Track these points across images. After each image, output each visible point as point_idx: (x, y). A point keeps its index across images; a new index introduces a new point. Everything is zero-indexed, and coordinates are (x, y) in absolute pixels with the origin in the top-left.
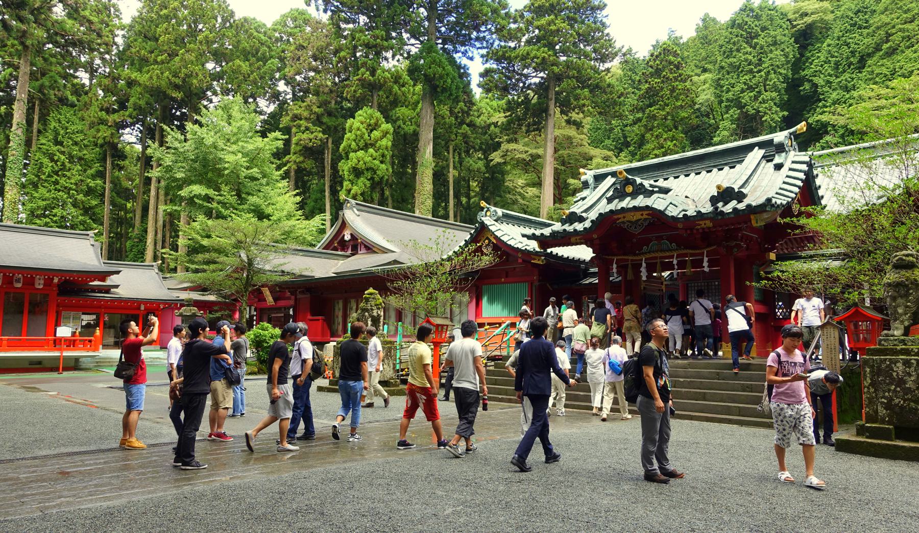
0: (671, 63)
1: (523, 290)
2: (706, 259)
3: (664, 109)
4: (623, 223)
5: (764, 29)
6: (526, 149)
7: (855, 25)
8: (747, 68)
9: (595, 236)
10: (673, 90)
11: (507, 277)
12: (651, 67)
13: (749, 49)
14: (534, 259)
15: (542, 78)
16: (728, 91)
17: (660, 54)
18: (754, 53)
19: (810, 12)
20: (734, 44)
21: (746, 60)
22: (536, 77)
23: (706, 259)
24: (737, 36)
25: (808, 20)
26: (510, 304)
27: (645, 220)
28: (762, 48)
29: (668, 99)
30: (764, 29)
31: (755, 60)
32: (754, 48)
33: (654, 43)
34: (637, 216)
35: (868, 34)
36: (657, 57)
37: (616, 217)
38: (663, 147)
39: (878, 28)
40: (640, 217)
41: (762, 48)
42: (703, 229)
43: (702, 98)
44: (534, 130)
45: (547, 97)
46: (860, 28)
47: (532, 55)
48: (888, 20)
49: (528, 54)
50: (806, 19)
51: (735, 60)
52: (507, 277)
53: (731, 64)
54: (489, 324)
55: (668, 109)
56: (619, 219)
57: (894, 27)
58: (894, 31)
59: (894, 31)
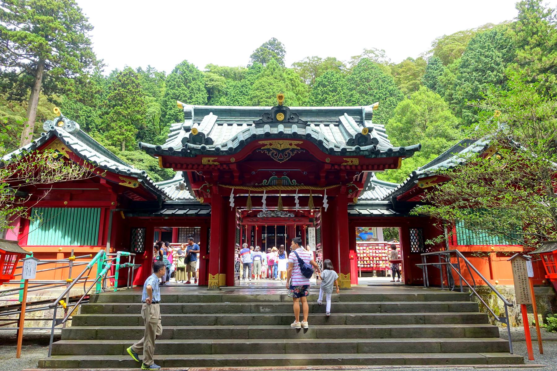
0: (133, 82)
1: (93, 216)
2: (326, 196)
3: (126, 110)
4: (269, 150)
5: (194, 79)
6: (4, 113)
7: (241, 92)
8: (183, 99)
9: (233, 160)
10: (133, 100)
11: (71, 199)
12: (120, 81)
13: (185, 88)
14: (123, 181)
15: (33, 61)
16: (171, 109)
17: (127, 74)
18: (188, 91)
19: (215, 79)
20: (177, 82)
21: (184, 94)
22: (27, 58)
23: (326, 196)
24: (179, 78)
25: (215, 84)
26: (70, 230)
27: (293, 150)
28: (192, 90)
29: (130, 104)
30: (194, 79)
31: (188, 95)
32: (188, 88)
33: (114, 70)
34: (284, 145)
35: (248, 99)
36: (125, 75)
37: (261, 142)
38: (123, 135)
39: (254, 97)
40: (289, 146)
41: (192, 90)
42: (351, 166)
43: (151, 110)
44: (16, 99)
45: (35, 76)
46: (244, 94)
47: (29, 39)
48: (259, 94)
49: (26, 37)
50: (213, 82)
51: (177, 92)
52: (71, 199)
53: (174, 94)
54: (76, 254)
55: (129, 110)
56: (264, 145)
57: (262, 98)
58: (262, 100)
59: (262, 100)
